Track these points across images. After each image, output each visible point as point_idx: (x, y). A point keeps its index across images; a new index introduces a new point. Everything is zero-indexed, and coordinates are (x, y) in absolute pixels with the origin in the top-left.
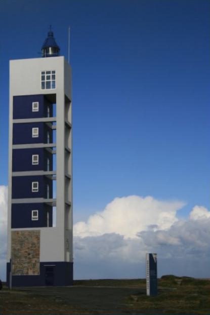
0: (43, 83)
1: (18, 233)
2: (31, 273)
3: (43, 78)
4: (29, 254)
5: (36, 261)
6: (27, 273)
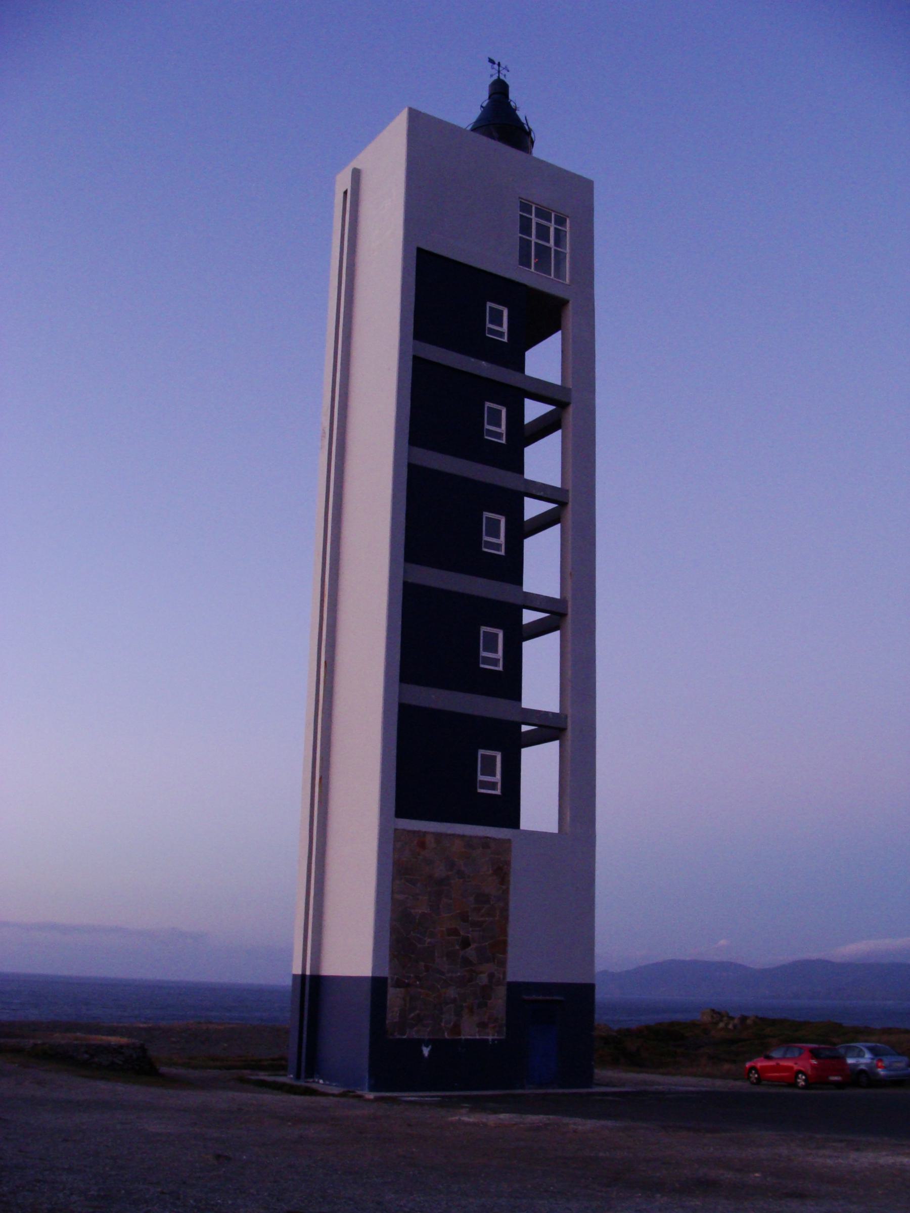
0: (525, 246)
1: (422, 845)
2: (469, 1031)
3: (525, 226)
4: (466, 943)
5: (491, 976)
6: (456, 1029)
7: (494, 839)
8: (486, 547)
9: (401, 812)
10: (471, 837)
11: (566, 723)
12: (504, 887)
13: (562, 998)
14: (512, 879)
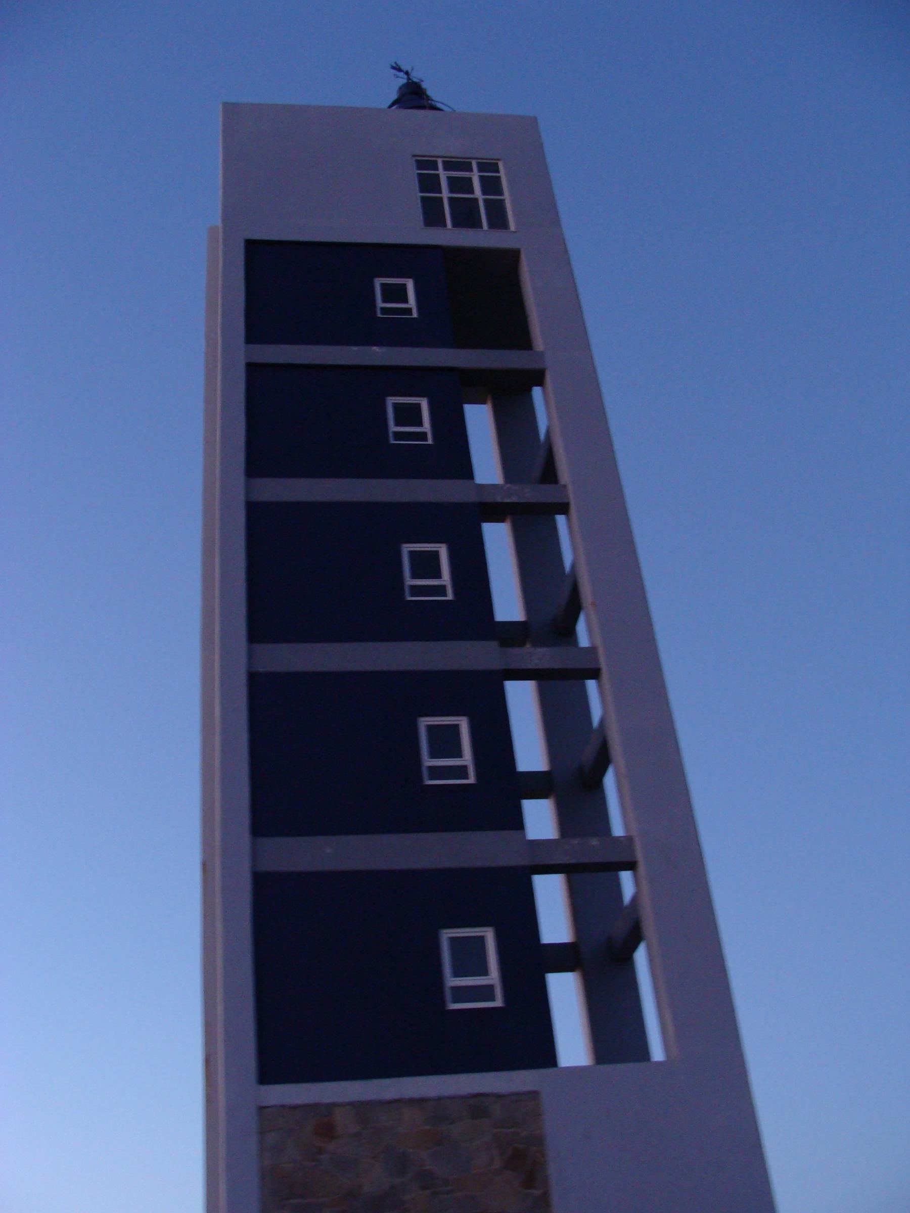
1: (327, 1130)
3: (429, 183)
7: (499, 1096)
8: (455, 1001)
9: (268, 1074)
10: (439, 1099)
11: (597, 660)
12: (537, 1192)
13: (657, 1053)
14: (553, 1170)
